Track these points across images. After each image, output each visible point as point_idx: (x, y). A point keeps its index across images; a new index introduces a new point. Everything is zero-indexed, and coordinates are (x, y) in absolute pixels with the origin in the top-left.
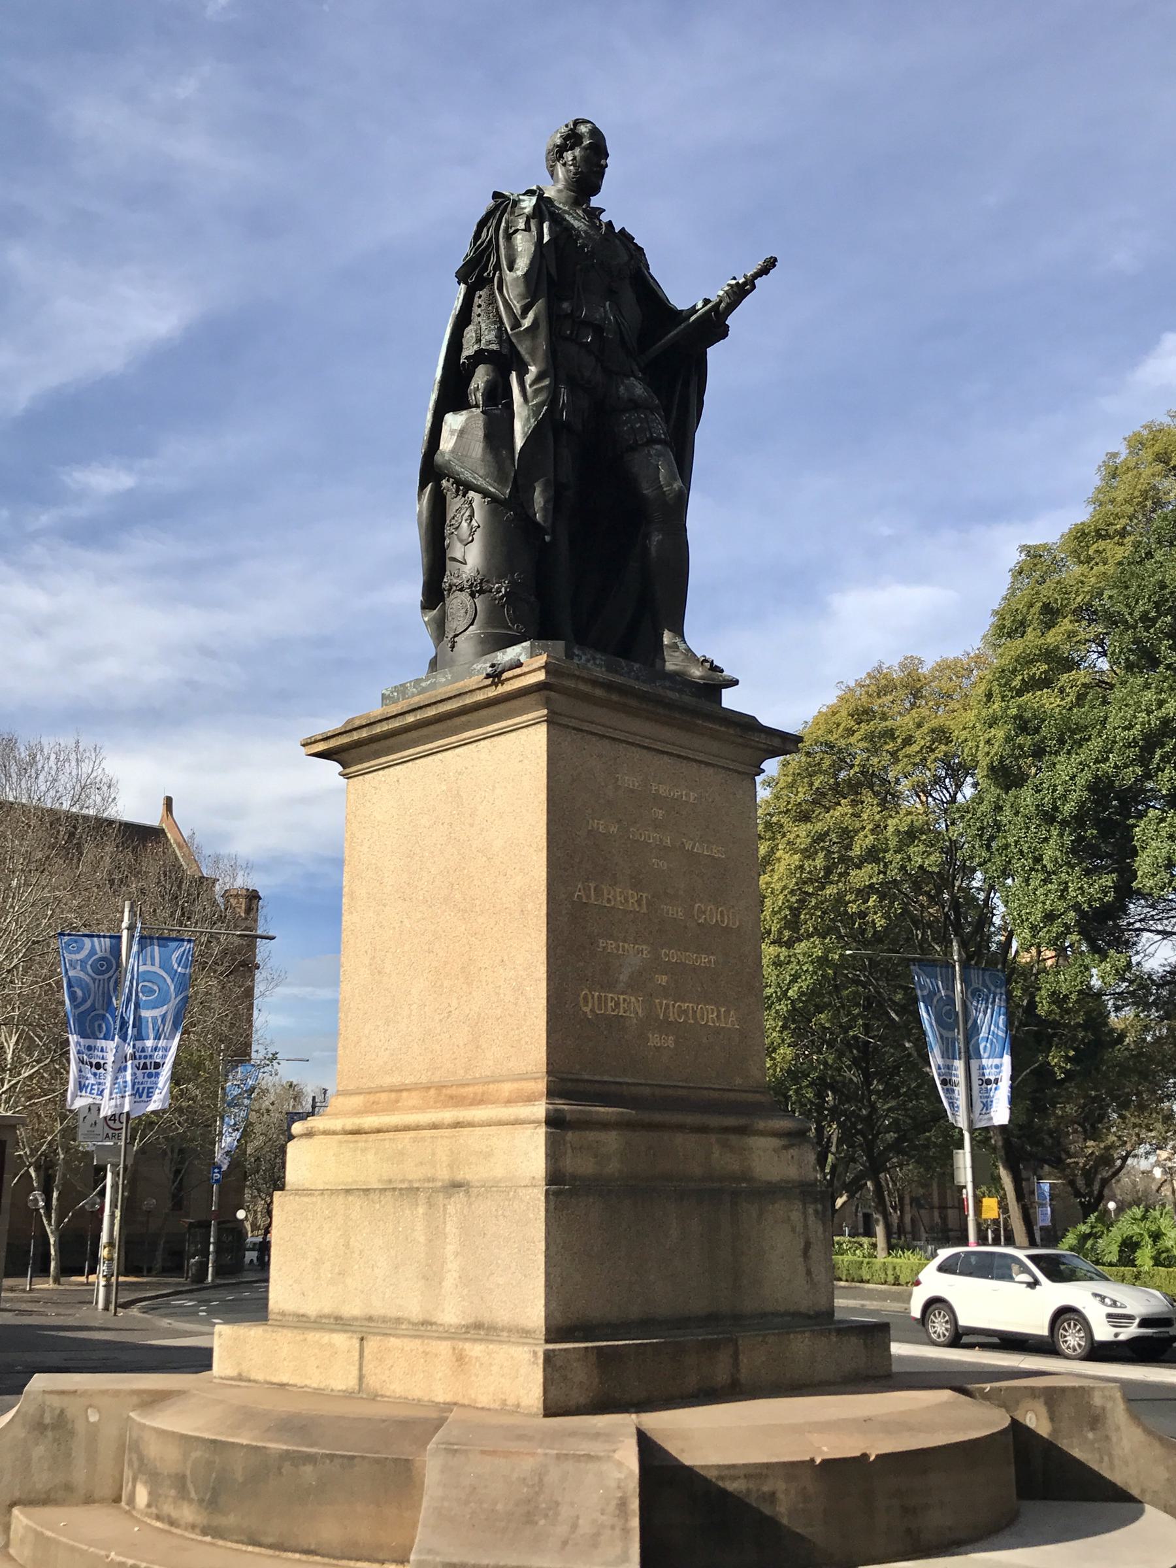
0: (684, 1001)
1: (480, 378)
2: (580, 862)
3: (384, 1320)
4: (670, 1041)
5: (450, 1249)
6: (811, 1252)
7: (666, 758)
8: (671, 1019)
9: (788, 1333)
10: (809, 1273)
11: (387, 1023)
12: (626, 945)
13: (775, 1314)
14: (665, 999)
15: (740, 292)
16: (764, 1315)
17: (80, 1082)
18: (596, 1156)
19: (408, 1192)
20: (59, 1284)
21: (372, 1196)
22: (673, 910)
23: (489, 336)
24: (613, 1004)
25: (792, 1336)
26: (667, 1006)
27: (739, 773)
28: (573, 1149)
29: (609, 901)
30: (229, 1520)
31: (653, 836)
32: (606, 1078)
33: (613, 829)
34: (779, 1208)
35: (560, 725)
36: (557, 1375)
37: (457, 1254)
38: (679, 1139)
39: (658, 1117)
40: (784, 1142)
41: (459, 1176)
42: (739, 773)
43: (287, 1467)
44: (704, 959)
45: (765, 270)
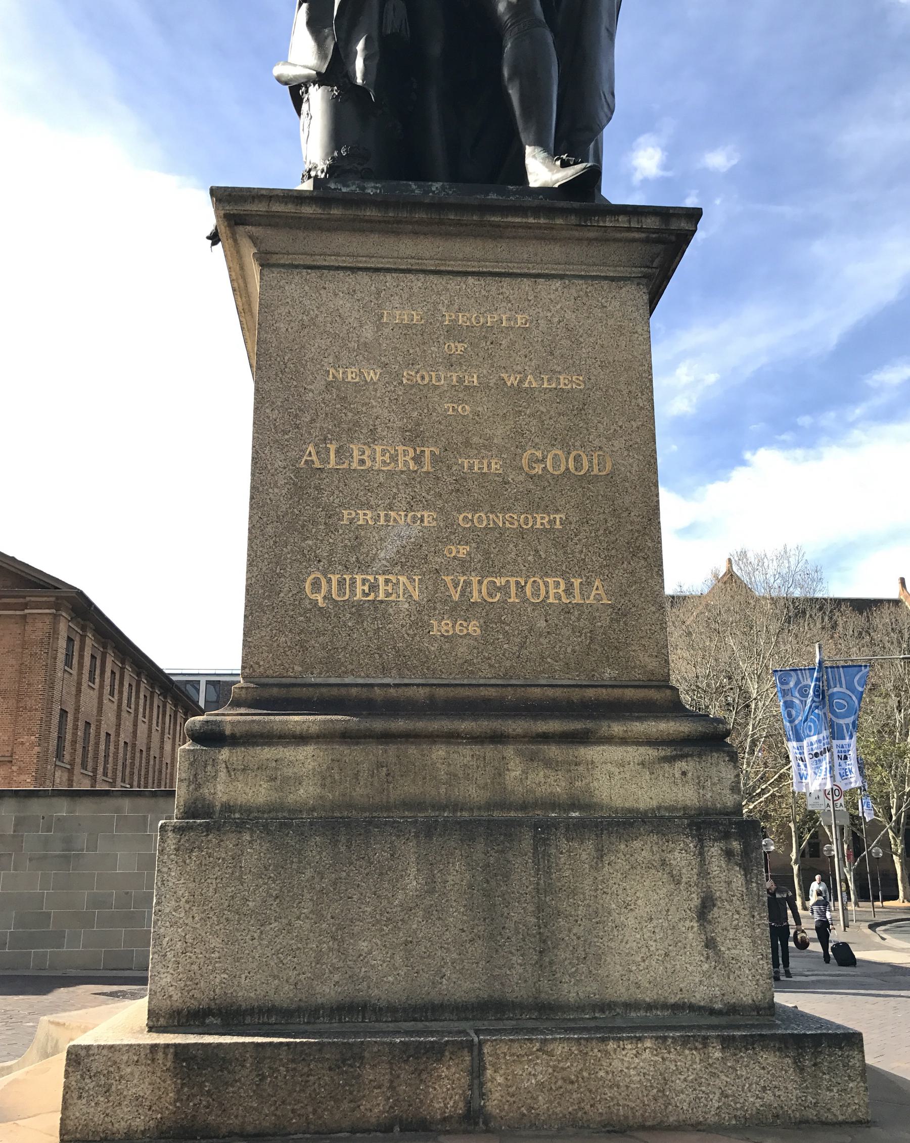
2: (313, 421)
4: (474, 628)
7: (471, 280)
8: (475, 597)
9: (603, 1040)
10: (710, 944)
13: (630, 1006)
14: (464, 574)
16: (605, 1006)
17: (800, 773)
18: (273, 779)
20: (858, 907)
22: (481, 463)
24: (366, 588)
25: (612, 1045)
26: (468, 584)
27: (612, 279)
31: (444, 378)
32: (347, 680)
33: (372, 375)
35: (283, 266)
36: (90, 1084)
38: (439, 752)
39: (420, 725)
40: (668, 751)
42: (612, 279)
44: (541, 520)
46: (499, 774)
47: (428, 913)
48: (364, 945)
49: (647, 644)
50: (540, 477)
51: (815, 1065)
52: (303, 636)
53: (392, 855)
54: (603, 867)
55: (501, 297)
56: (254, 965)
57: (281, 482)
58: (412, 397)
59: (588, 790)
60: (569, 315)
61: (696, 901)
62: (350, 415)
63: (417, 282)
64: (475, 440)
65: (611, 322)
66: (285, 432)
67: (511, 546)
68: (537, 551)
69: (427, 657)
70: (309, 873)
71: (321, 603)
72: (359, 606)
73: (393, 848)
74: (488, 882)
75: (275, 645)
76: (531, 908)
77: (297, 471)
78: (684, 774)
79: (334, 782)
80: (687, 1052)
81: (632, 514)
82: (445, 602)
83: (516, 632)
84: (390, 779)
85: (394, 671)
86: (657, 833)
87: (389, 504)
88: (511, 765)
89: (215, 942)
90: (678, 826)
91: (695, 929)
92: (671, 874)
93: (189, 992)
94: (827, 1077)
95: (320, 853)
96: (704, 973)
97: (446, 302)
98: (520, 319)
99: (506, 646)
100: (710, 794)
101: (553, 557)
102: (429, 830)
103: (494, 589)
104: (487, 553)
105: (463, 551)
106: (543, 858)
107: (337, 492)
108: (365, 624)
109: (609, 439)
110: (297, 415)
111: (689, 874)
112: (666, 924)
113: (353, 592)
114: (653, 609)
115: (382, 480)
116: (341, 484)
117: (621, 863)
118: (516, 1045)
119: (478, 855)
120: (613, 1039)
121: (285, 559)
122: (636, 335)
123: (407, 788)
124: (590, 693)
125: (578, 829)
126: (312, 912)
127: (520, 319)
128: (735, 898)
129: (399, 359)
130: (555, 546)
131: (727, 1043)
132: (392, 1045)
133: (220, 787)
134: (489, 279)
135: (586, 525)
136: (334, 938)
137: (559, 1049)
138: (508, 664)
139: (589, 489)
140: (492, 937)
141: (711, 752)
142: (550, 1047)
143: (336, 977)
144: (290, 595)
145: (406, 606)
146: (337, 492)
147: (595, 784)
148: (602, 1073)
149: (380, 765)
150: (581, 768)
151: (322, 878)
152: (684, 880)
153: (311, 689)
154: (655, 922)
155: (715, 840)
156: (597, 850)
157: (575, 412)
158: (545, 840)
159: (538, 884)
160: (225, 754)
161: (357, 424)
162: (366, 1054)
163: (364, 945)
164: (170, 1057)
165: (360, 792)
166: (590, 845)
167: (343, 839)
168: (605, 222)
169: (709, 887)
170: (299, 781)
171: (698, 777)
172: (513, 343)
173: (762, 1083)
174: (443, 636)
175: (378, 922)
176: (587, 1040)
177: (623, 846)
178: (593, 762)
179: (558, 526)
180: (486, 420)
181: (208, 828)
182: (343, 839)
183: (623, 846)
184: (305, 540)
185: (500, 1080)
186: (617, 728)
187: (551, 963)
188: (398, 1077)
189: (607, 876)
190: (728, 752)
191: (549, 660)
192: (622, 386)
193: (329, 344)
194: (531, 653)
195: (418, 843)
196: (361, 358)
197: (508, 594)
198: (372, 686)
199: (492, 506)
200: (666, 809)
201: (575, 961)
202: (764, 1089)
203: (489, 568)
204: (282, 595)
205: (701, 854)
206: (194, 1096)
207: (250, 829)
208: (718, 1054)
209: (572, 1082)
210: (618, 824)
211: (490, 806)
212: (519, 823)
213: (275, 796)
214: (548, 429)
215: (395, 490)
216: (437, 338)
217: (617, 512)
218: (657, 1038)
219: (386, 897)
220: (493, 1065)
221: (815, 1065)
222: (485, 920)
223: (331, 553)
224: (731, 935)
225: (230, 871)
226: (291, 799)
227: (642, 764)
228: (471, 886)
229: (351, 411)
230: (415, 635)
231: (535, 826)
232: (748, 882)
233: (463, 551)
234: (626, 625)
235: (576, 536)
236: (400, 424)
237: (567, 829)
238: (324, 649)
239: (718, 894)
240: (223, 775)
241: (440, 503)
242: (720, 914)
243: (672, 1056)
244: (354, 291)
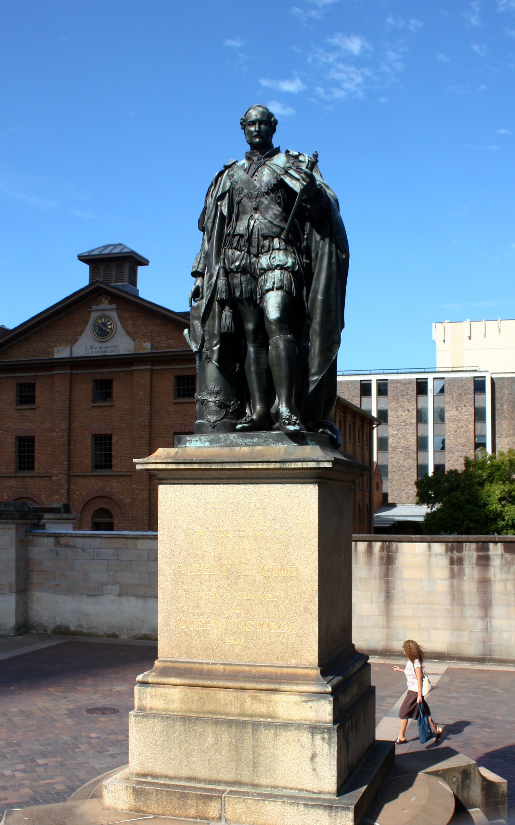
10: (314, 770)
18: (165, 700)
25: (266, 802)
34: (292, 734)
46: (243, 703)
47: (216, 750)
48: (195, 759)
49: (309, 650)
50: (269, 577)
51: (335, 815)
52: (179, 642)
53: (204, 730)
54: (277, 740)
55: (254, 494)
56: (161, 762)
57: (169, 580)
58: (218, 542)
62: (194, 550)
64: (243, 561)
66: (171, 558)
67: (257, 607)
68: (267, 610)
69: (224, 652)
73: (204, 728)
74: (236, 742)
75: (169, 645)
76: (251, 752)
78: (311, 707)
79: (185, 702)
80: (292, 807)
81: (306, 594)
82: (231, 631)
83: (258, 644)
84: (204, 703)
85: (212, 658)
86: (297, 730)
87: (210, 589)
88: (247, 701)
89: (148, 753)
90: (305, 728)
91: (309, 764)
92: (301, 744)
93: (141, 768)
94: (340, 820)
95: (180, 728)
96: (311, 779)
97: (232, 497)
99: (254, 649)
100: (320, 715)
101: (273, 612)
102: (216, 722)
104: (247, 610)
106: (256, 735)
107: (190, 584)
108: (201, 638)
110: (174, 551)
112: (298, 762)
114: (313, 635)
115: (207, 579)
116: (191, 581)
118: (235, 799)
120: (267, 800)
121: (172, 611)
122: (312, 511)
123: (210, 707)
124: (285, 670)
125: (268, 726)
126: (178, 747)
128: (324, 755)
129: (213, 524)
130: (274, 608)
131: (306, 805)
132: (197, 794)
133: (148, 701)
135: (287, 598)
136: (185, 756)
137: (249, 802)
138: (254, 656)
139: (289, 582)
140: (237, 760)
141: (322, 699)
142: (246, 801)
143: (186, 768)
144: (174, 626)
145: (216, 632)
146: (190, 584)
147: (277, 709)
148: (263, 811)
149: (201, 698)
150: (272, 703)
151: (181, 736)
152: (306, 747)
153: (181, 664)
154: (294, 761)
155: (318, 734)
156: (275, 734)
157: (284, 548)
158: (256, 729)
159: (253, 744)
160: (149, 690)
161: (196, 554)
162: (189, 796)
163: (195, 759)
164: (132, 789)
165: (194, 707)
167: (187, 724)
168: (291, 466)
169: (315, 750)
170: (174, 701)
171: (316, 709)
173: (317, 819)
174: (230, 644)
175: (200, 752)
176: (258, 800)
177: (284, 733)
178: (277, 701)
180: (247, 552)
181: (144, 716)
182: (187, 724)
183: (284, 733)
184: (178, 604)
185: (230, 809)
186: (287, 688)
187: (257, 771)
188: (199, 804)
189: (278, 743)
190: (328, 700)
191: (270, 655)
193: (185, 519)
194: (263, 652)
195: (212, 727)
196: (198, 525)
198: (202, 663)
199: (249, 590)
200: (304, 720)
201: (265, 771)
202: (317, 821)
204: (171, 626)
206: (139, 802)
207: (157, 717)
208: (303, 809)
209: (253, 812)
210: (283, 725)
211: (239, 715)
212: (245, 722)
213: (166, 706)
214: (273, 555)
215: (211, 583)
216: (228, 514)
217: (300, 593)
218: (282, 802)
219: (202, 744)
220: (228, 804)
221: (335, 815)
222: (235, 755)
224: (322, 767)
225: (152, 731)
226: (171, 707)
227: (295, 703)
228: (230, 743)
229: (194, 548)
230: (219, 643)
231: (253, 724)
232: (330, 749)
234: (301, 642)
235: (283, 603)
236: (213, 554)
237: (264, 726)
238: (186, 648)
239: (318, 753)
240: (149, 697)
241: (229, 588)
243: (287, 808)
244: (195, 494)
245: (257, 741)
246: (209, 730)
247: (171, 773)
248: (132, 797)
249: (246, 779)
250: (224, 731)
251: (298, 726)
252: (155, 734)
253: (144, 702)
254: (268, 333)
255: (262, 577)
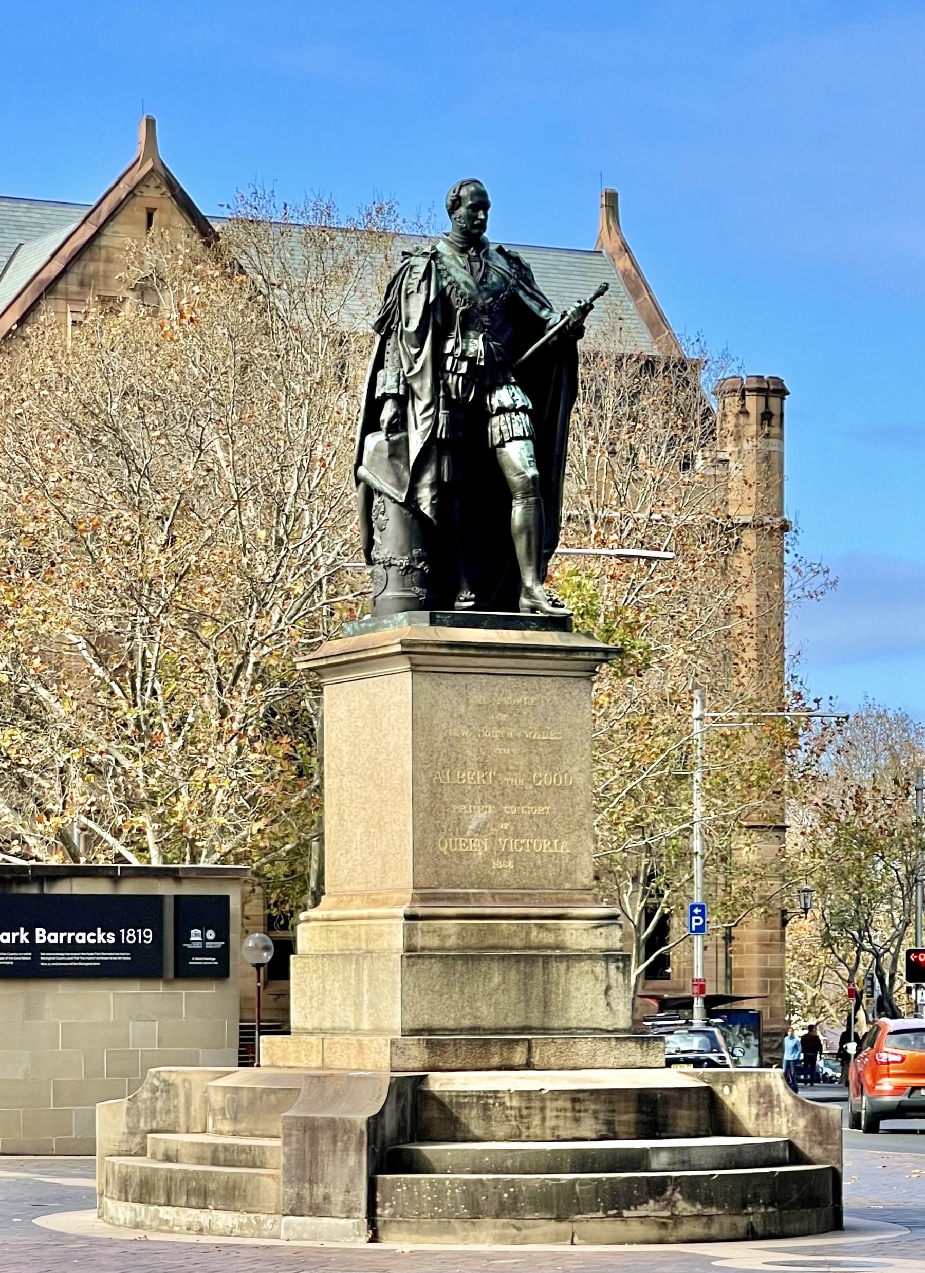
0: (522, 838)
1: (388, 411)
3: (340, 1029)
5: (366, 988)
6: (611, 992)
10: (608, 1004)
11: (346, 853)
12: (475, 807)
15: (584, 311)
18: (439, 936)
19: (346, 956)
21: (334, 958)
23: (391, 381)
28: (423, 932)
29: (461, 779)
30: (242, 1126)
31: (497, 733)
34: (586, 966)
37: (368, 991)
41: (371, 947)
43: (265, 1097)
44: (540, 810)
45: (599, 294)
48: (479, 1004)
59: (563, 941)
60: (555, 698)
61: (604, 988)
63: (484, 679)
64: (511, 767)
65: (574, 702)
70: (458, 975)
71: (446, 853)
72: (460, 853)
73: (489, 965)
77: (431, 785)
98: (533, 699)
103: (520, 845)
105: (506, 826)
109: (571, 766)
111: (602, 976)
113: (459, 847)
117: (576, 972)
119: (522, 968)
127: (533, 699)
134: (518, 678)
160: (420, 923)
165: (473, 941)
166: (565, 964)
170: (449, 936)
172: (528, 714)
179: (548, 813)
192: (578, 738)
197: (525, 848)
203: (517, 835)
205: (607, 968)
223: (448, 827)
233: (506, 826)
242: (613, 993)
245: (548, 975)
246: (495, 965)
247: (451, 1024)
248: (426, 1052)
249: (535, 1023)
250: (511, 967)
251: (589, 956)
252: (432, 978)
253: (414, 941)
254: (512, 491)
255: (531, 787)
